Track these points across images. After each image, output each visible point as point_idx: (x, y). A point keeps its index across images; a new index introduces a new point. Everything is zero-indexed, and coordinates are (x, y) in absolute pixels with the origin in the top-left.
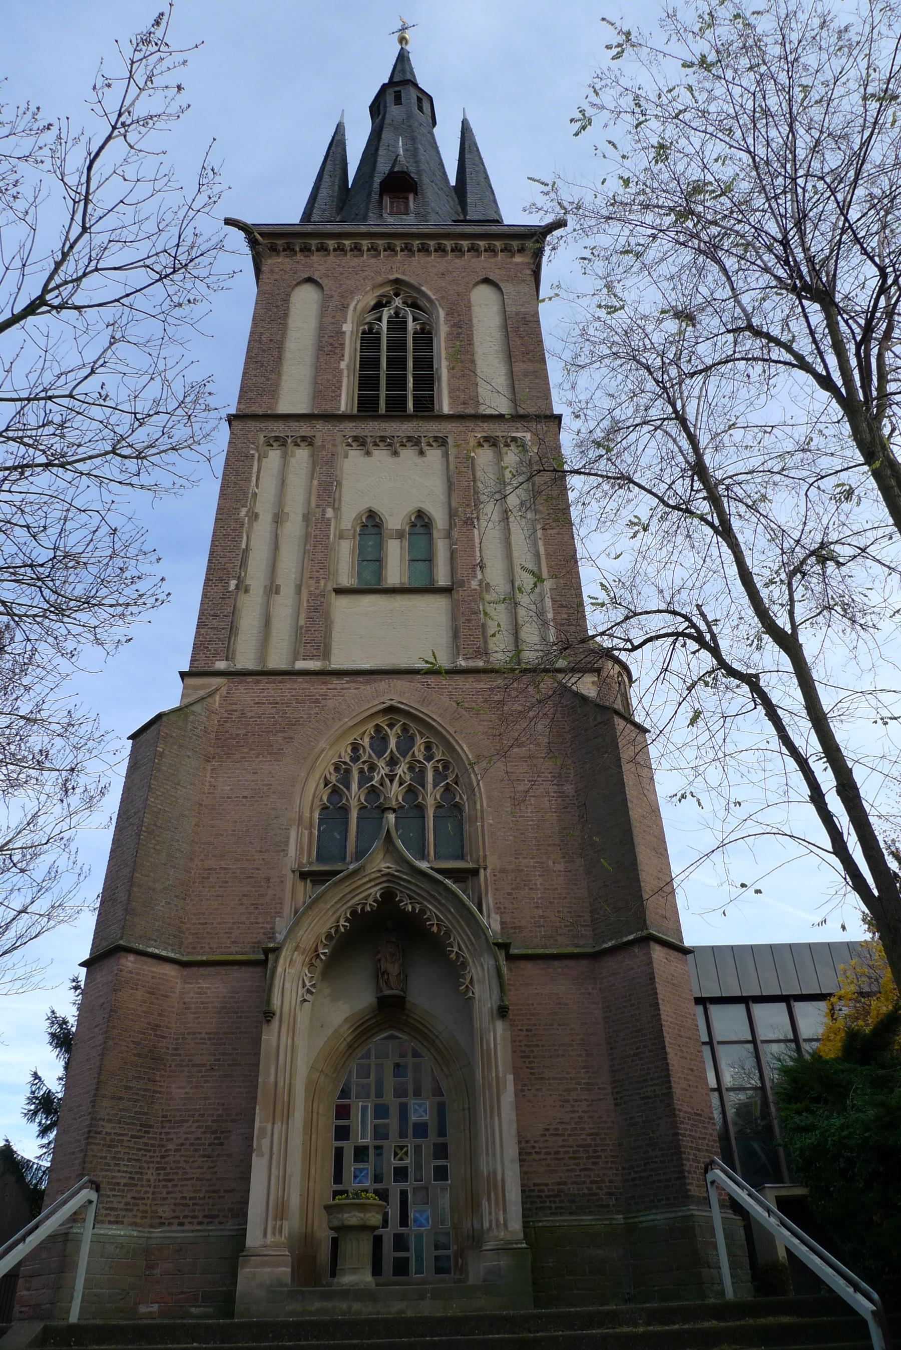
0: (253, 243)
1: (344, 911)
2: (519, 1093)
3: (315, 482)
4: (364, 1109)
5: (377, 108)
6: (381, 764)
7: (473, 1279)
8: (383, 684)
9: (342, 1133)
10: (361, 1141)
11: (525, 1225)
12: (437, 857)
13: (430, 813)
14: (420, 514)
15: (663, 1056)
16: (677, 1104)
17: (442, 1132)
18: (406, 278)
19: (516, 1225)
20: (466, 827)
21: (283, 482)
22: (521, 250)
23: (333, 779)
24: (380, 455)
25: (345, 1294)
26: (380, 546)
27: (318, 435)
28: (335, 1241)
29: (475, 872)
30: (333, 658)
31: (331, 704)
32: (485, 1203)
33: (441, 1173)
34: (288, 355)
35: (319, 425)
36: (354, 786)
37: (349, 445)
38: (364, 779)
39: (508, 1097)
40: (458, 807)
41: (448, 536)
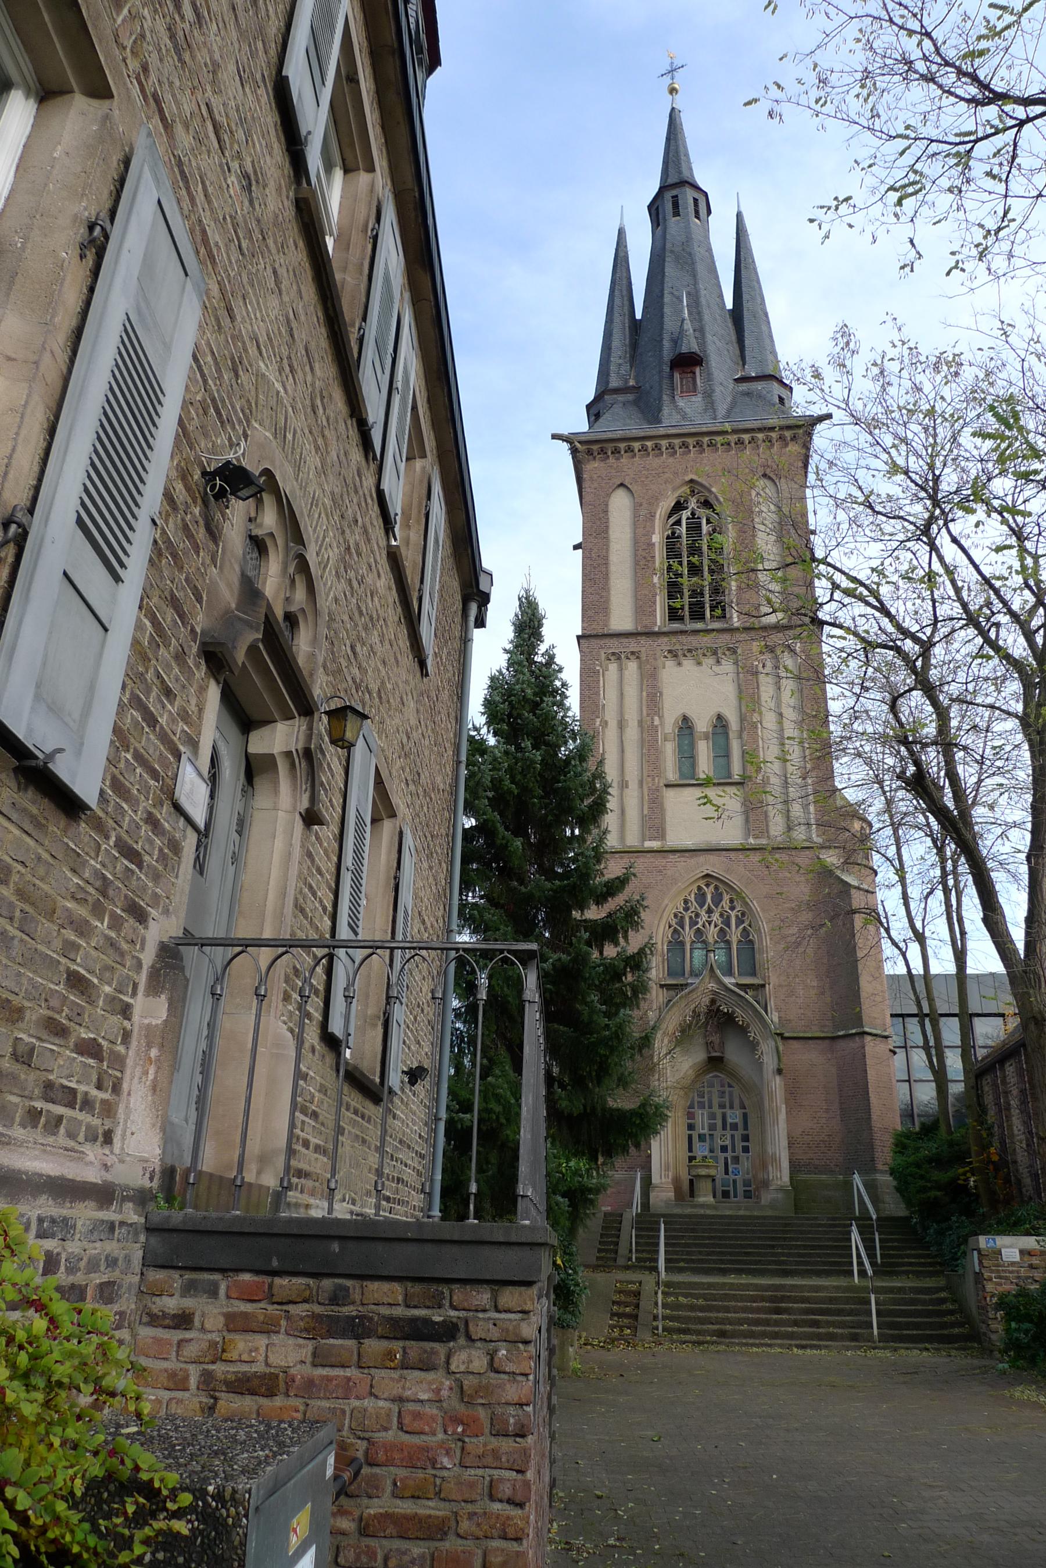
0: (574, 451)
1: (689, 1012)
2: (788, 1113)
3: (644, 694)
4: (703, 1114)
5: (655, 208)
6: (703, 913)
7: (763, 1202)
8: (702, 858)
9: (691, 1127)
10: (702, 1132)
11: (791, 1178)
12: (740, 974)
13: (734, 946)
14: (719, 717)
15: (868, 1100)
16: (873, 1124)
17: (746, 1128)
18: (699, 480)
19: (786, 1179)
20: (757, 956)
21: (622, 694)
22: (794, 438)
23: (673, 923)
24: (688, 664)
25: (703, 1206)
26: (692, 746)
27: (643, 650)
28: (691, 1182)
29: (763, 986)
30: (668, 838)
31: (669, 873)
32: (770, 1168)
33: (746, 1150)
34: (613, 568)
35: (643, 640)
36: (687, 928)
37: (665, 657)
38: (693, 923)
39: (782, 1116)
40: (751, 942)
41: (740, 737)
